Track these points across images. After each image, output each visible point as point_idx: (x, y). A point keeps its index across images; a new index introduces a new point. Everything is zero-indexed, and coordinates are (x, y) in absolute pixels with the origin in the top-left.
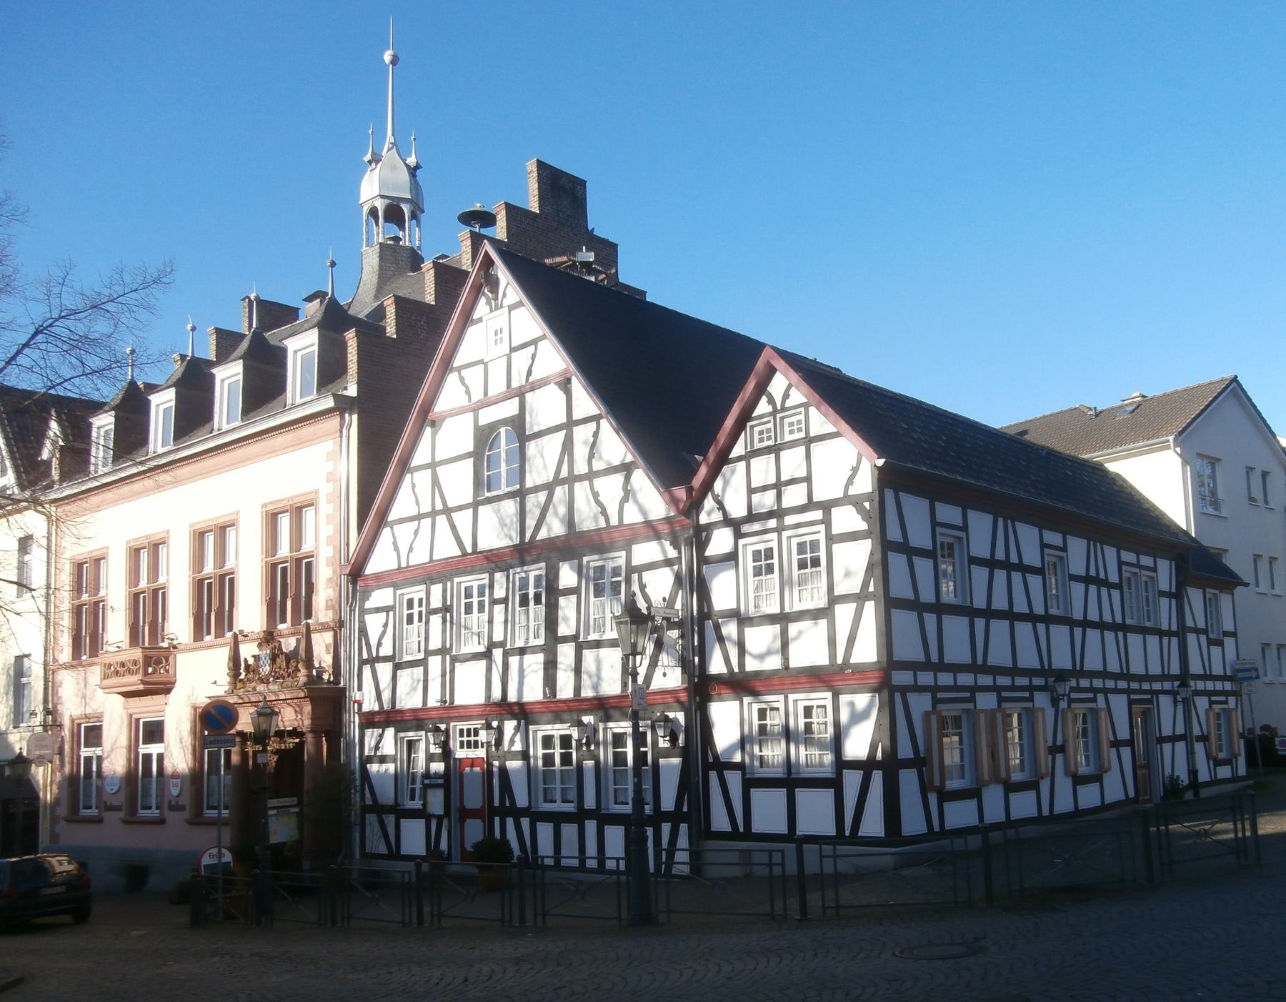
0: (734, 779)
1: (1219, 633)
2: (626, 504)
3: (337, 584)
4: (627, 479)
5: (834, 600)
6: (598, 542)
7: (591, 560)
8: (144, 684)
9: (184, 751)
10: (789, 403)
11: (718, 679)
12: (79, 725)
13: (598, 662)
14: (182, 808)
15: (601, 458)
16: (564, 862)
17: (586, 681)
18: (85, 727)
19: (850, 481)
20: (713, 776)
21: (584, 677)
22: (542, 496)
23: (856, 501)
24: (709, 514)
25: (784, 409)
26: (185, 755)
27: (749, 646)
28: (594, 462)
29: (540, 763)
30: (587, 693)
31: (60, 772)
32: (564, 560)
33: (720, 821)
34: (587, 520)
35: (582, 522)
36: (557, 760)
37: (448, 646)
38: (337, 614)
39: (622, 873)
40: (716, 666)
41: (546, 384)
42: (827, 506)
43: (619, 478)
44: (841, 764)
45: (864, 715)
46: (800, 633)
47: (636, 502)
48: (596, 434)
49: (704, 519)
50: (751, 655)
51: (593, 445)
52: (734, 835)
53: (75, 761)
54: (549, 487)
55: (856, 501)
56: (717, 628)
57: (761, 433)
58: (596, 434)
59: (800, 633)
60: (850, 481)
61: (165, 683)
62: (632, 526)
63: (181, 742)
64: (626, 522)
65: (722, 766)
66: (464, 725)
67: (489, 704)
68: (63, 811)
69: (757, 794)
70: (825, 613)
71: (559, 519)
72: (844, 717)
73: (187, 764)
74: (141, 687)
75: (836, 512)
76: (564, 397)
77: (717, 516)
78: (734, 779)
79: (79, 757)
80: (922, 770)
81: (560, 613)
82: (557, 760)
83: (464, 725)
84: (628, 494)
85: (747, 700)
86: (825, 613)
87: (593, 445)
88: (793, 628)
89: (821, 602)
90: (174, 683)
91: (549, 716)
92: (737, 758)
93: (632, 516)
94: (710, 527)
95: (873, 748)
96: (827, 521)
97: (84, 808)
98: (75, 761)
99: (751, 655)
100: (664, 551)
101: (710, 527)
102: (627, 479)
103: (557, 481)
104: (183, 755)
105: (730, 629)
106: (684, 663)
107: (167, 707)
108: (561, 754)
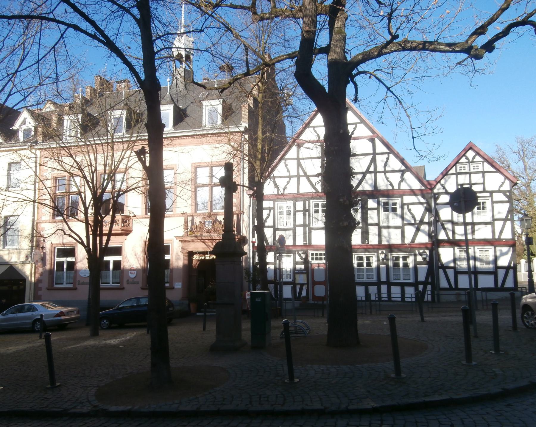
0: (451, 273)
1: (146, 218)
2: (402, 183)
3: (239, 198)
4: (402, 175)
5: (494, 220)
6: (387, 194)
7: (382, 200)
8: (121, 230)
9: (138, 259)
10: (475, 160)
11: (443, 241)
12: (55, 248)
13: (389, 234)
14: (137, 283)
15: (389, 166)
16: (383, 299)
17: (383, 239)
18: (57, 249)
19: (501, 186)
20: (441, 271)
21: (383, 238)
22: (360, 177)
23: (504, 192)
24: (438, 190)
25: (473, 162)
26: (138, 261)
27: (456, 231)
28: (386, 167)
29: (356, 266)
30: (384, 242)
31: (42, 267)
32: (370, 198)
33: (444, 284)
34: (382, 185)
35: (380, 186)
36: (365, 265)
37: (307, 223)
38: (238, 208)
39: (414, 302)
40: (442, 236)
41: (363, 138)
42: (491, 193)
43: (399, 174)
44: (497, 268)
45: (506, 253)
46: (479, 229)
47: (406, 182)
48: (388, 159)
49: (436, 191)
50: (458, 234)
51: (386, 162)
52: (450, 288)
53: (52, 263)
54: (364, 174)
55: (504, 192)
56: (443, 225)
57: (461, 167)
58: (388, 159)
59: (479, 229)
60: (501, 186)
61: (128, 231)
62: (404, 190)
63: (136, 256)
64: (401, 188)
65: (444, 268)
66: (315, 252)
67: (305, 245)
68: (45, 285)
69: (460, 277)
70: (491, 223)
71: (369, 185)
72: (498, 254)
73: (140, 265)
74: (120, 232)
75: (494, 195)
76: (371, 144)
77: (442, 191)
78: (451, 273)
79: (54, 261)
80: (259, 259)
81: (369, 216)
82: (365, 265)
83: (315, 252)
84: (402, 180)
85: (456, 248)
86: (491, 223)
87: (386, 162)
88: (476, 227)
89: (489, 219)
90: (131, 231)
91: (362, 250)
92: (452, 265)
93: (404, 186)
94: (439, 194)
95: (510, 263)
96: (491, 196)
97: (56, 284)
98: (52, 263)
99: (458, 234)
100: (418, 199)
101: (439, 194)
102: (402, 175)
103: (368, 171)
104: (137, 261)
105: (449, 226)
106: (430, 235)
107: (125, 241)
108: (367, 263)
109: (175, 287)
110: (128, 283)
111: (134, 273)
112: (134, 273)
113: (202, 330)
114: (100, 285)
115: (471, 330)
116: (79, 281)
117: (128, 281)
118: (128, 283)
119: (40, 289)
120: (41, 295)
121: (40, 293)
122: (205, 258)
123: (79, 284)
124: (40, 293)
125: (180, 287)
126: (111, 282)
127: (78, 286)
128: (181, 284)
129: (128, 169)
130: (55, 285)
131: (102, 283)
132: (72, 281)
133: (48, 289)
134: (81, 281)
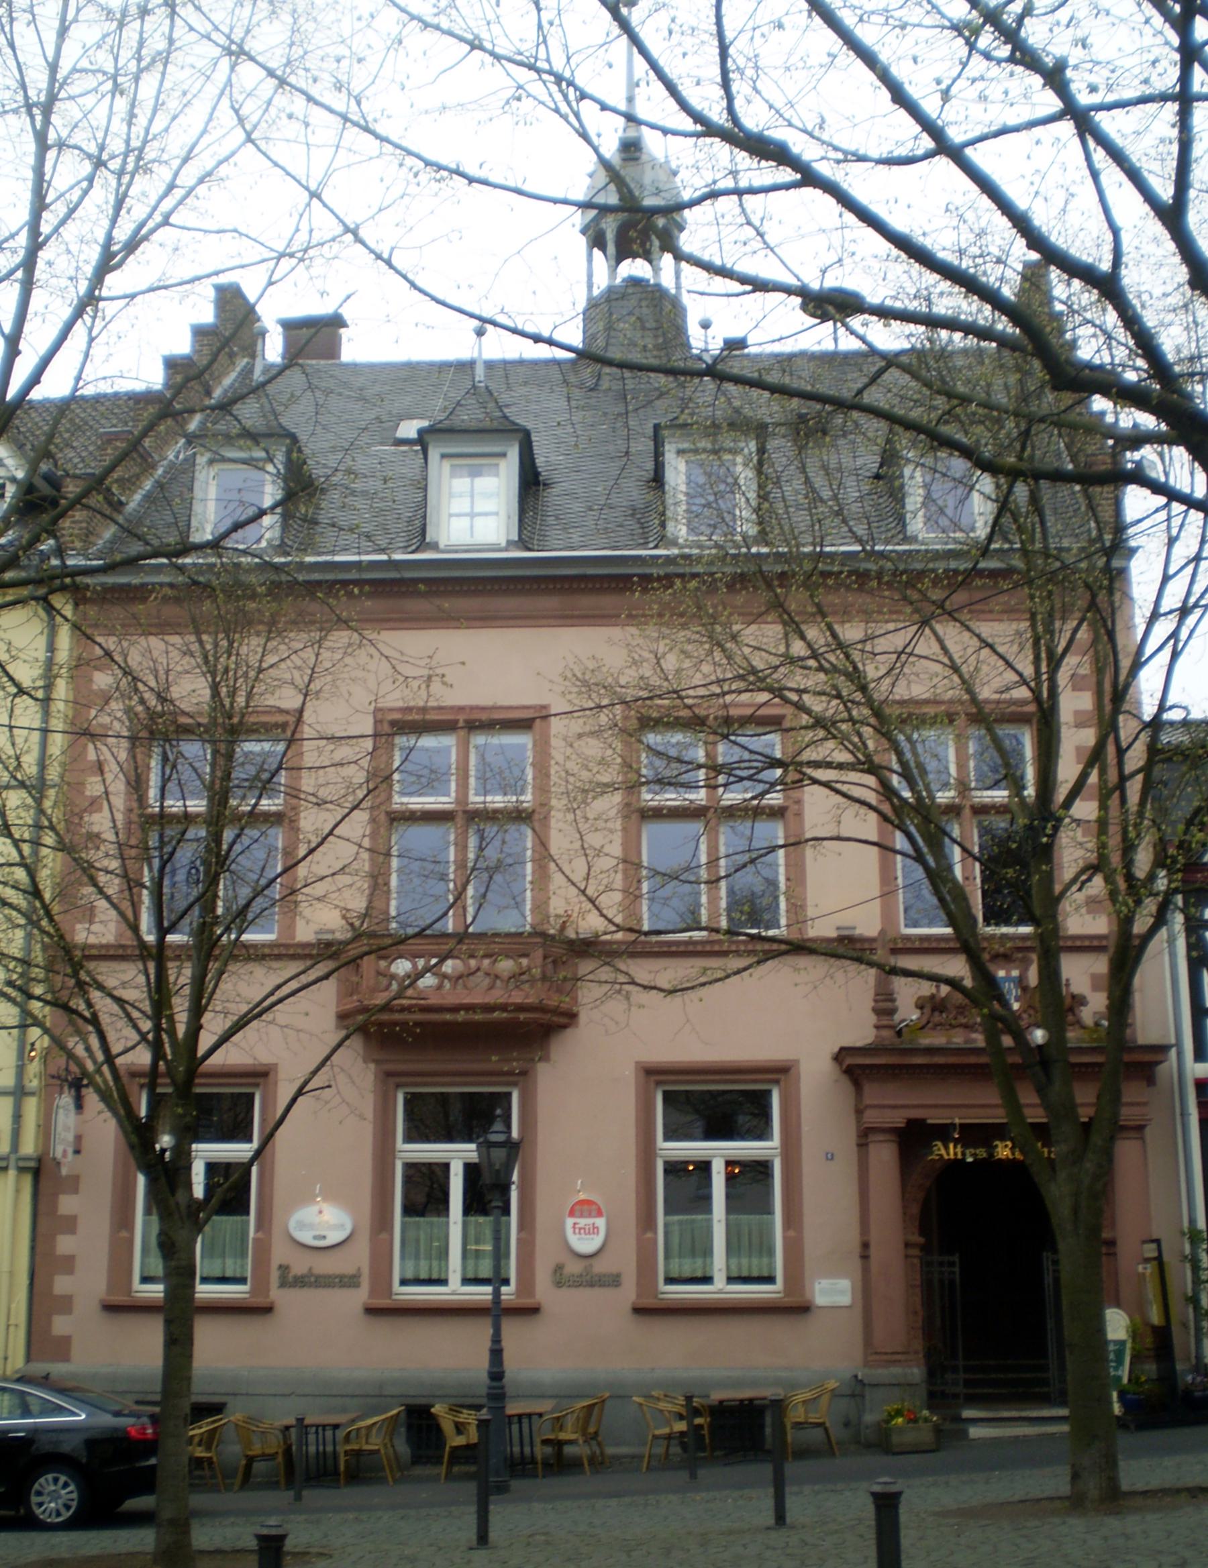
14: (614, 1281)
61: (556, 1011)
109: (820, 1300)
110: (559, 1284)
111: (595, 1229)
112: (595, 1229)
113: (771, 1521)
114: (193, 1286)
115: (1168, 1462)
116: (284, 1269)
117: (559, 1268)
118: (559, 1284)
119: (65, 1304)
120: (66, 1341)
121: (61, 1325)
122: (991, 1155)
123: (283, 1284)
124: (61, 1325)
125: (845, 1300)
126: (455, 1278)
127: (276, 1294)
128: (845, 1284)
129: (956, 620)
130: (396, 1287)
131: (205, 1280)
132: (486, 1270)
133: (111, 1308)
134: (299, 1267)
